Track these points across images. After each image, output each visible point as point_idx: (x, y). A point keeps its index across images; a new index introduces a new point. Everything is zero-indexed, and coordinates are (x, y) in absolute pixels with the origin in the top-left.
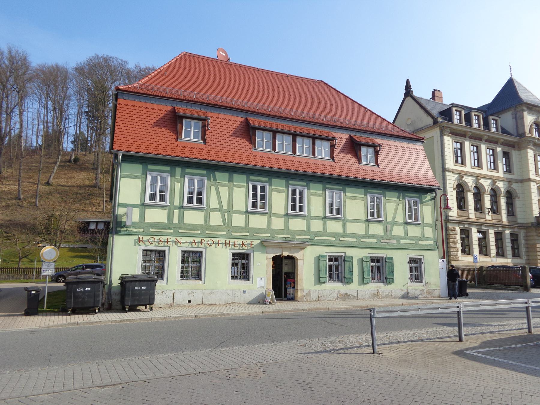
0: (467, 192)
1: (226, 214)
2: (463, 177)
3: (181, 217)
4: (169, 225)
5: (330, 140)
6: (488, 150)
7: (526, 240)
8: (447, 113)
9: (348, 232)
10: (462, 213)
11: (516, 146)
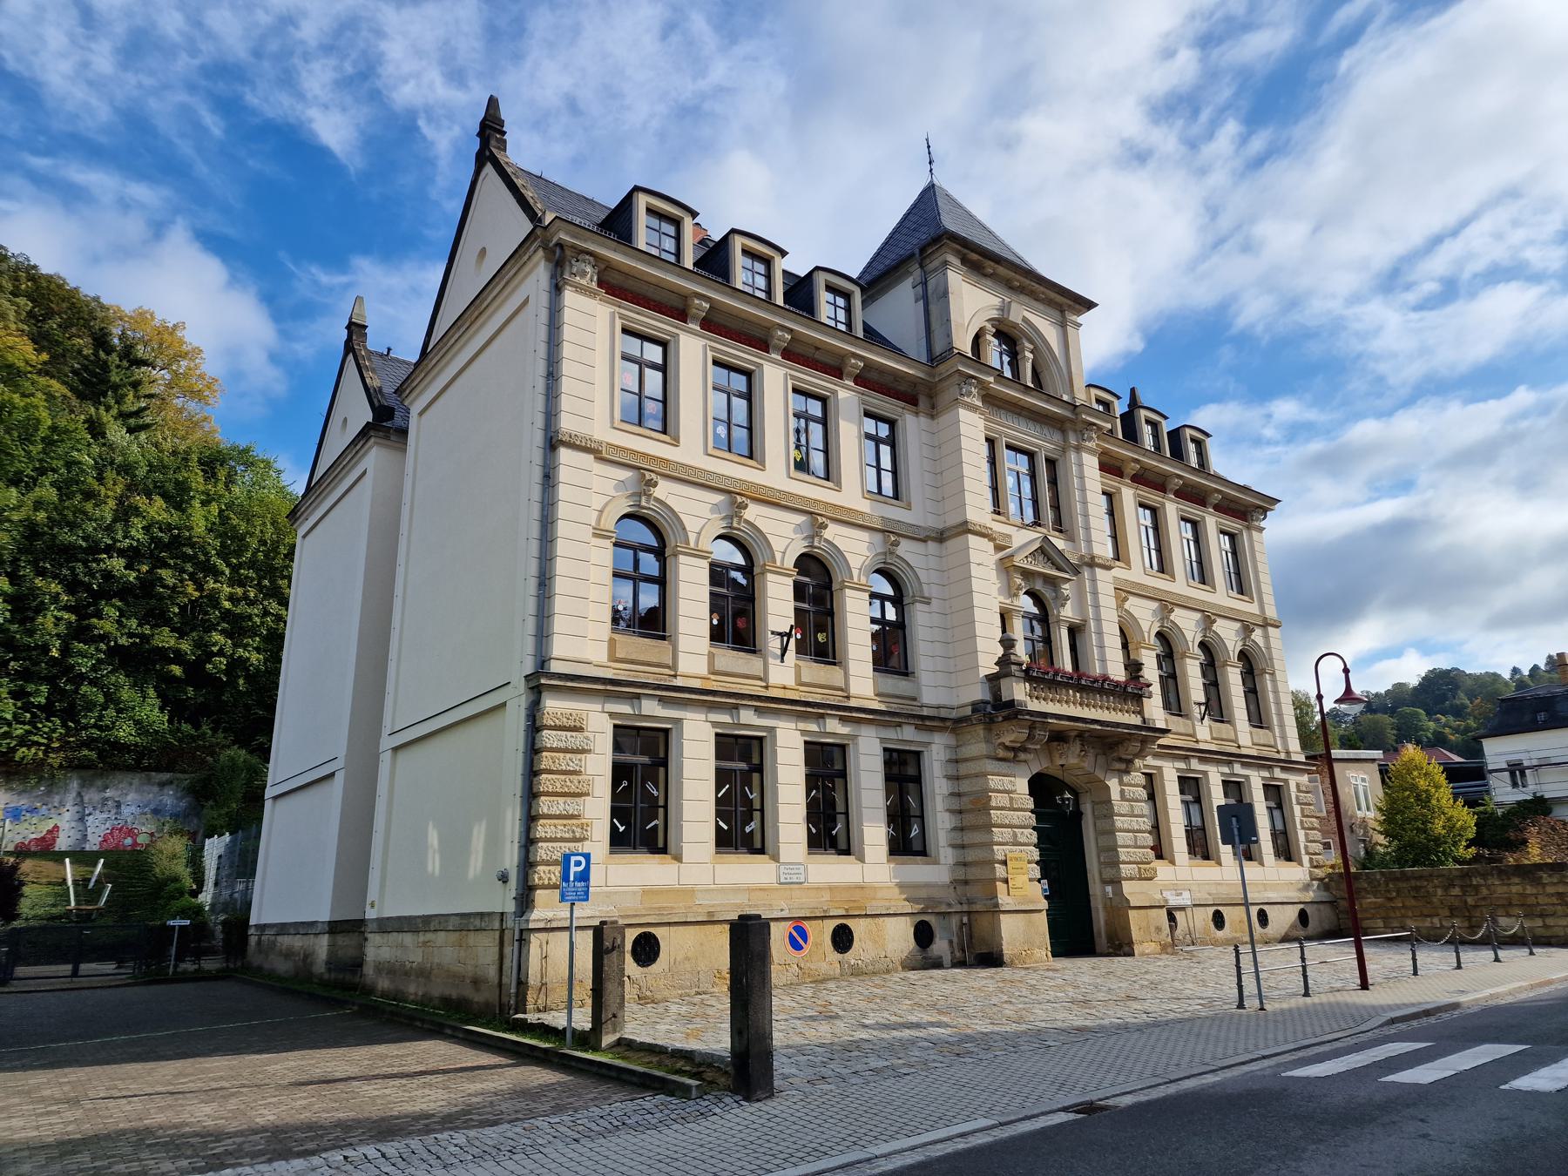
0: (675, 555)
2: (1172, 611)
6: (1141, 510)
7: (955, 778)
8: (715, 259)
10: (894, 684)
11: (923, 401)
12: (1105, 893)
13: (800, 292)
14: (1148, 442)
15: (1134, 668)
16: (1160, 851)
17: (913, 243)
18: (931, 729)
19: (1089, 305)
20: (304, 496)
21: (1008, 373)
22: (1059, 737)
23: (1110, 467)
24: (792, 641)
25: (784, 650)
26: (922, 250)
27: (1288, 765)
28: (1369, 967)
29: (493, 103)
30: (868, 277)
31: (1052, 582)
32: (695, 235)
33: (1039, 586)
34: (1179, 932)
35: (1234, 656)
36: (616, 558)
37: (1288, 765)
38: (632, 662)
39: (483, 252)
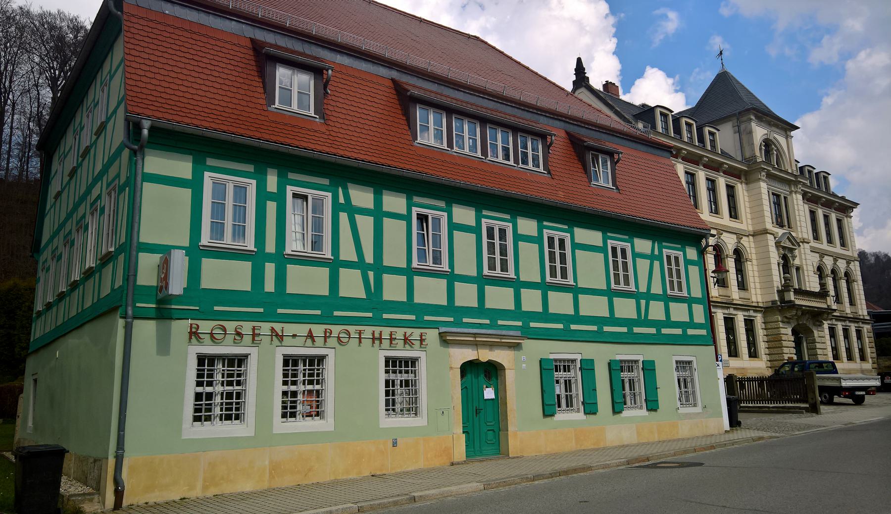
1: (371, 274)
3: (281, 278)
4: (255, 295)
5: (543, 136)
9: (552, 310)
15: (823, 285)
23: (809, 198)
27: (864, 321)
35: (731, 252)
37: (864, 321)
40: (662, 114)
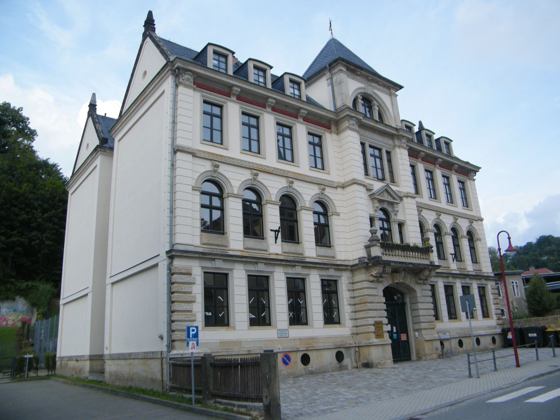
12: (415, 335)
13: (278, 82)
14: (426, 143)
15: (425, 240)
16: (437, 317)
17: (325, 62)
18: (341, 270)
19: (401, 87)
20: (71, 177)
21: (368, 115)
22: (395, 271)
23: (413, 154)
24: (280, 234)
25: (276, 238)
26: (330, 65)
28: (520, 358)
29: (150, 14)
30: (307, 76)
31: (391, 204)
32: (233, 61)
33: (385, 206)
34: (445, 350)
35: (465, 234)
36: (201, 199)
37: (487, 278)
38: (211, 245)
39: (145, 73)
40: (427, 135)
